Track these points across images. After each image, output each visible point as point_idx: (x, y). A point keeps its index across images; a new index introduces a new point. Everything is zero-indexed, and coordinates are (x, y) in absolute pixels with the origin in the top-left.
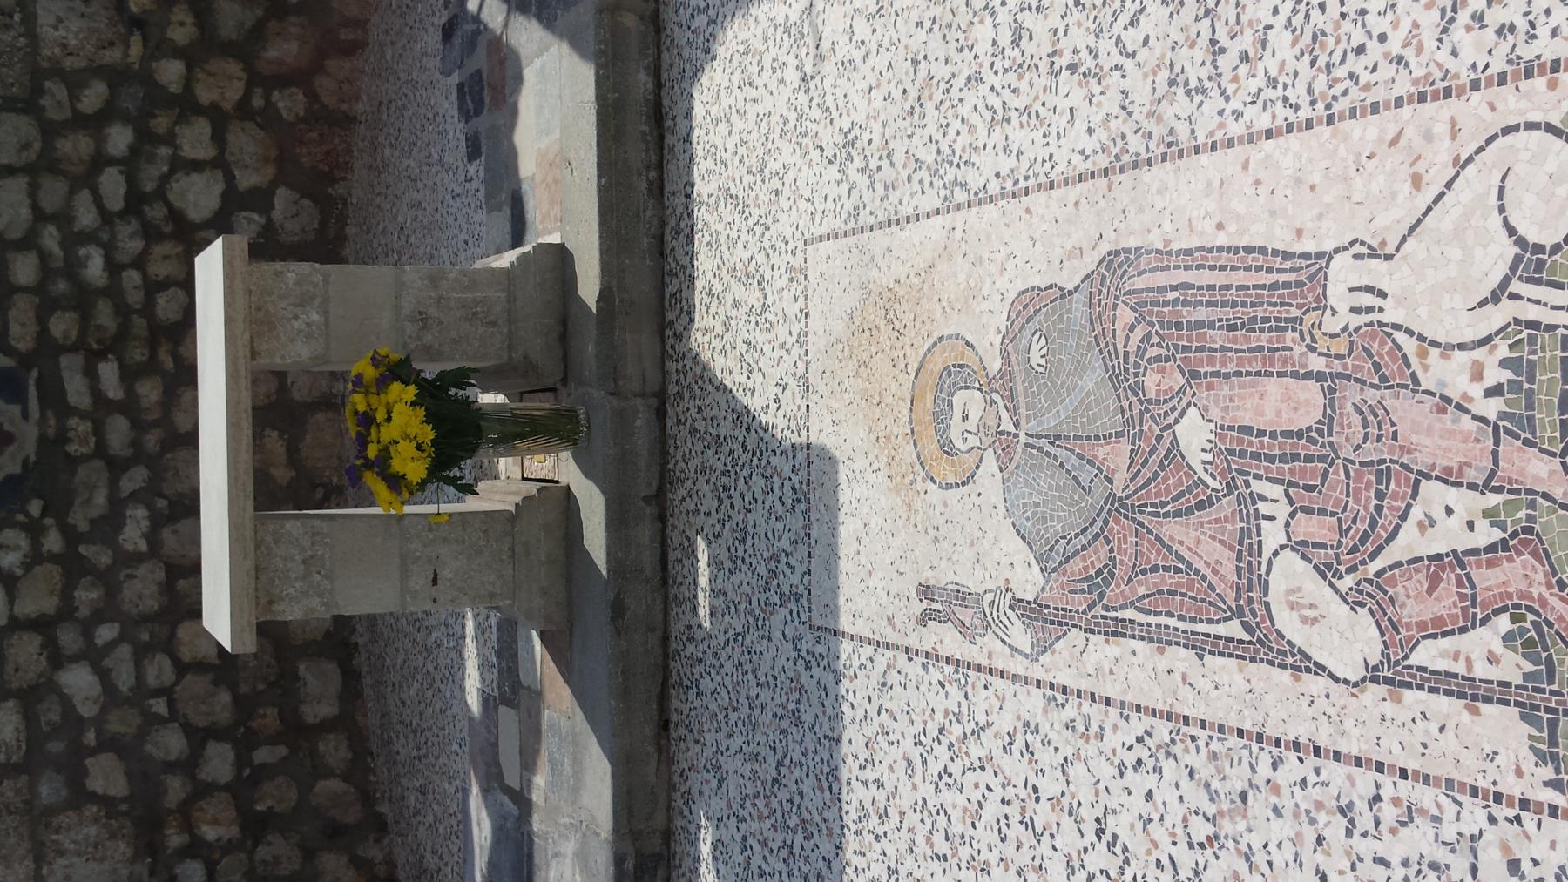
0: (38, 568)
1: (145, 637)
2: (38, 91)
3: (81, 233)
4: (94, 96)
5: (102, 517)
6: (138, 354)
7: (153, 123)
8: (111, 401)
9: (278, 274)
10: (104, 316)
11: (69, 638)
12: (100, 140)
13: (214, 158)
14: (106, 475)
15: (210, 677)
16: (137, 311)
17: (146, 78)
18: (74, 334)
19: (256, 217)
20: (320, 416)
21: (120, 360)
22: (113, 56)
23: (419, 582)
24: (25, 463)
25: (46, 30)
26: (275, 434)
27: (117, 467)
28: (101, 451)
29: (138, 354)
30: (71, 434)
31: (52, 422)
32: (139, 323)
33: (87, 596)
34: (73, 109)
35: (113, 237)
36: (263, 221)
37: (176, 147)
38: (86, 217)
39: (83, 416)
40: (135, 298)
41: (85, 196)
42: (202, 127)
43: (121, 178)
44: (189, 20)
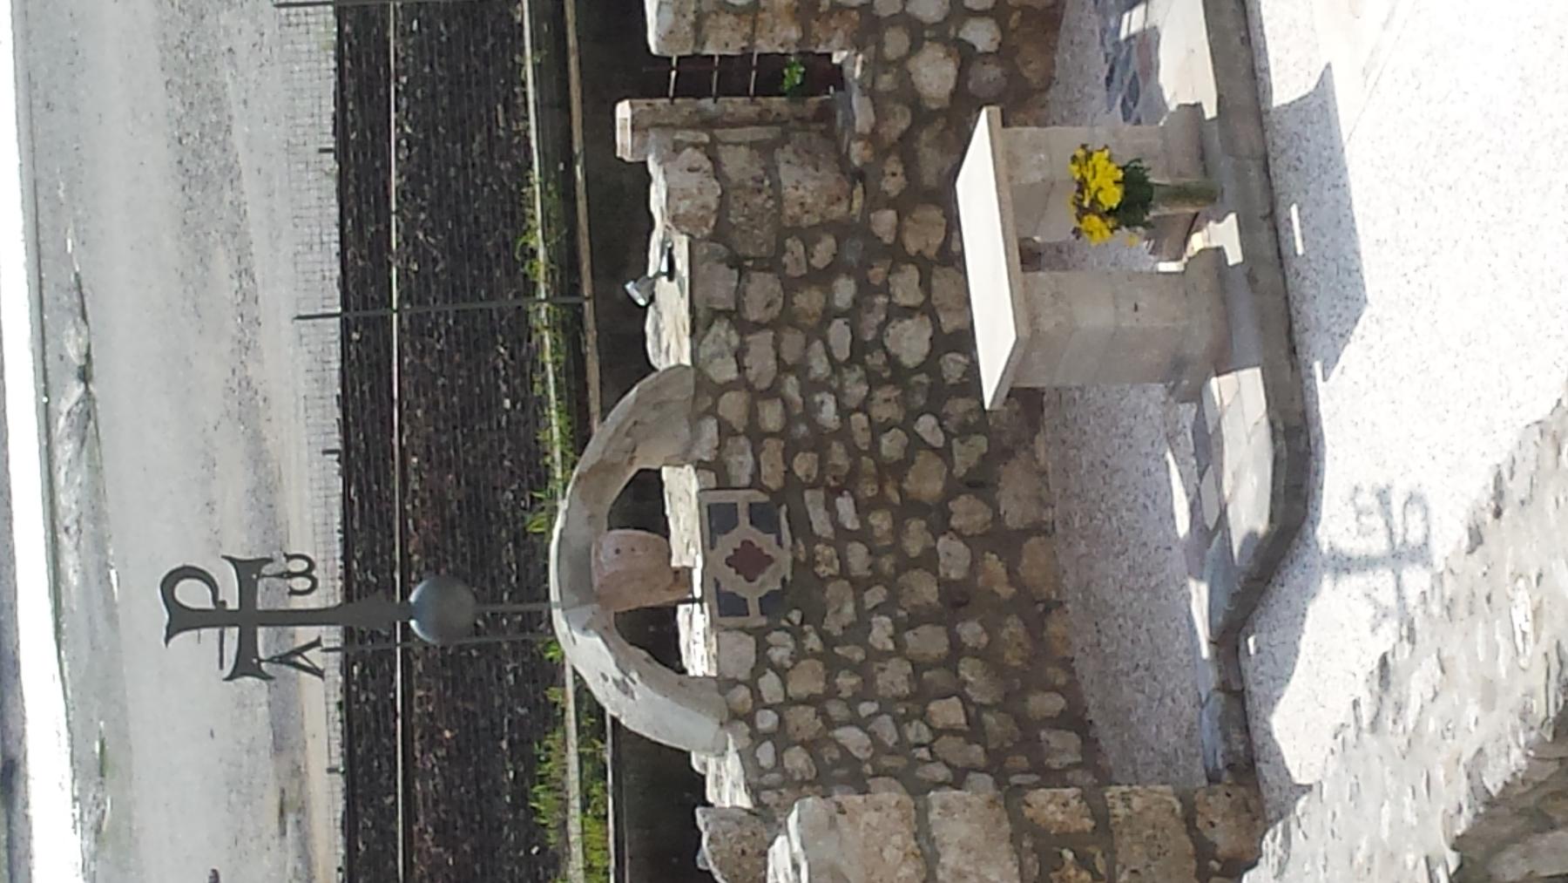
0: (803, 663)
1: (903, 711)
2: (782, 249)
3: (815, 382)
4: (824, 251)
5: (852, 624)
6: (869, 490)
7: (871, 273)
8: (850, 531)
9: (1017, 133)
10: (838, 456)
11: (836, 710)
12: (829, 296)
13: (923, 304)
14: (851, 594)
15: (961, 739)
16: (865, 453)
17: (864, 230)
18: (814, 474)
19: (960, 358)
20: (1034, 541)
21: (852, 494)
22: (839, 210)
23: (1127, 308)
24: (784, 580)
25: (789, 192)
26: (994, 557)
27: (859, 586)
28: (844, 572)
29: (869, 490)
30: (818, 558)
31: (802, 548)
32: (867, 463)
33: (847, 682)
34: (808, 263)
35: (841, 385)
36: (967, 361)
37: (890, 296)
38: (820, 367)
39: (828, 543)
40: (862, 439)
41: (818, 345)
42: (911, 274)
43: (847, 329)
44: (900, 170)
